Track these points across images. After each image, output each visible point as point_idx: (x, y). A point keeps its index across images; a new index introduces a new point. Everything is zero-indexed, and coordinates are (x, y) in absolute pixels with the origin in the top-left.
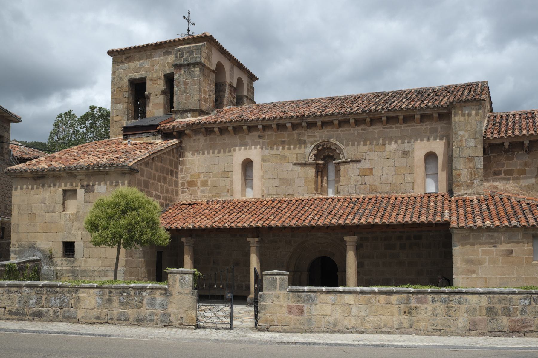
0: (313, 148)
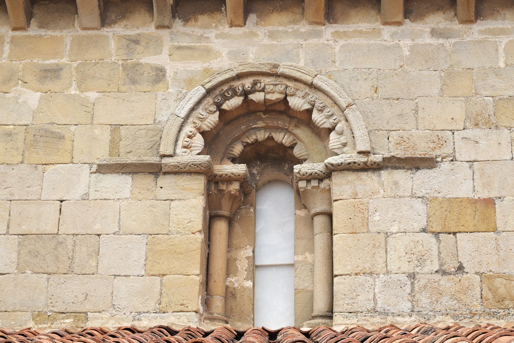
0: (199, 103)
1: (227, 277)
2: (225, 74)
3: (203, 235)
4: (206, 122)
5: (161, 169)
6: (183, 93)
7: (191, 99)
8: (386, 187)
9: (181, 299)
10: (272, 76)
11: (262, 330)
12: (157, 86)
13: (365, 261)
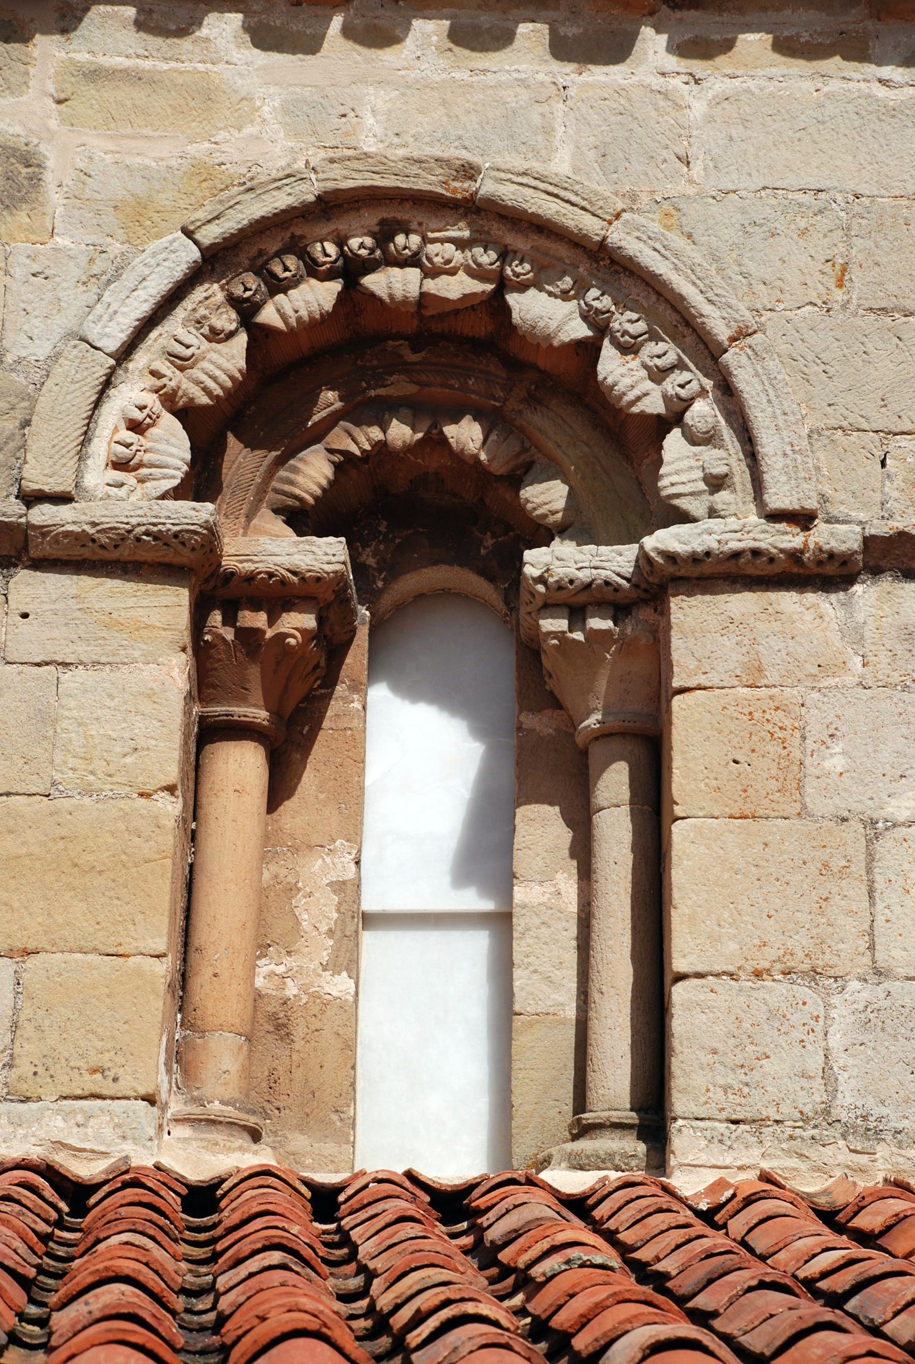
1: (259, 958)
2: (274, 193)
3: (181, 799)
4: (196, 373)
5: (26, 548)
6: (112, 257)
7: (145, 283)
8: (873, 648)
9: (94, 1047)
10: (451, 209)
11: (408, 1184)
12: (9, 219)
13: (791, 926)
